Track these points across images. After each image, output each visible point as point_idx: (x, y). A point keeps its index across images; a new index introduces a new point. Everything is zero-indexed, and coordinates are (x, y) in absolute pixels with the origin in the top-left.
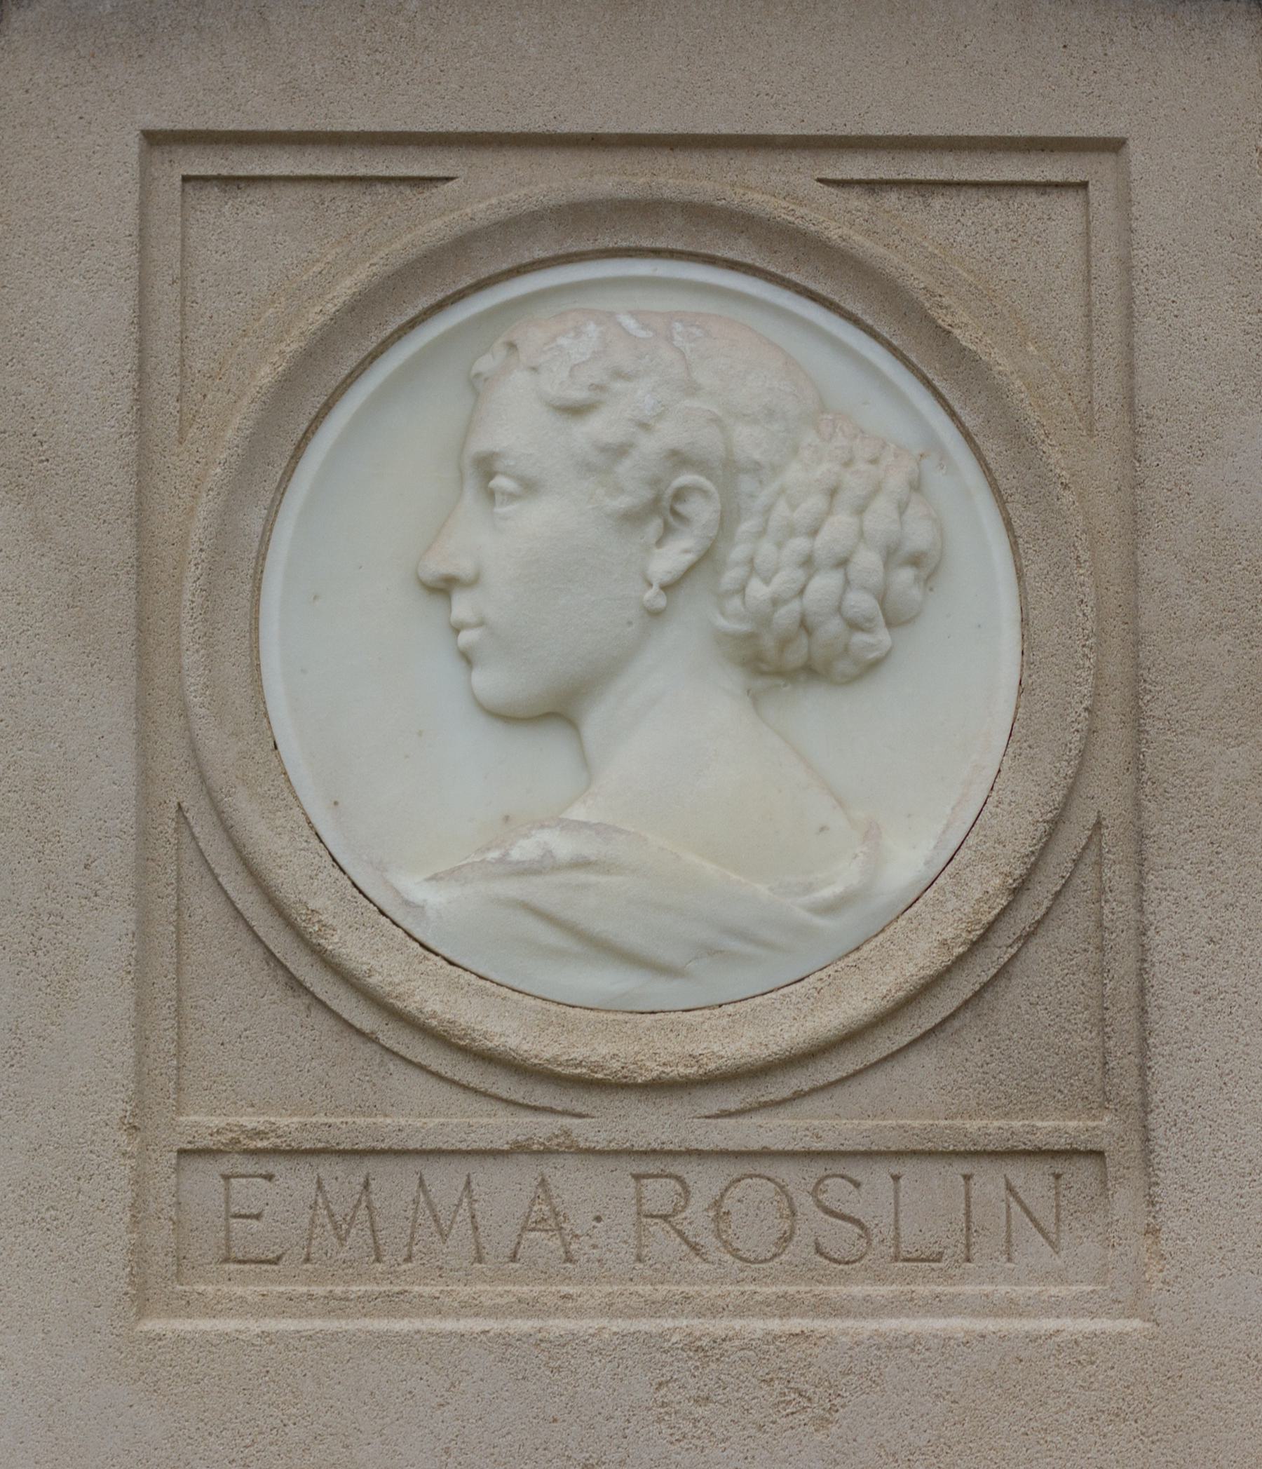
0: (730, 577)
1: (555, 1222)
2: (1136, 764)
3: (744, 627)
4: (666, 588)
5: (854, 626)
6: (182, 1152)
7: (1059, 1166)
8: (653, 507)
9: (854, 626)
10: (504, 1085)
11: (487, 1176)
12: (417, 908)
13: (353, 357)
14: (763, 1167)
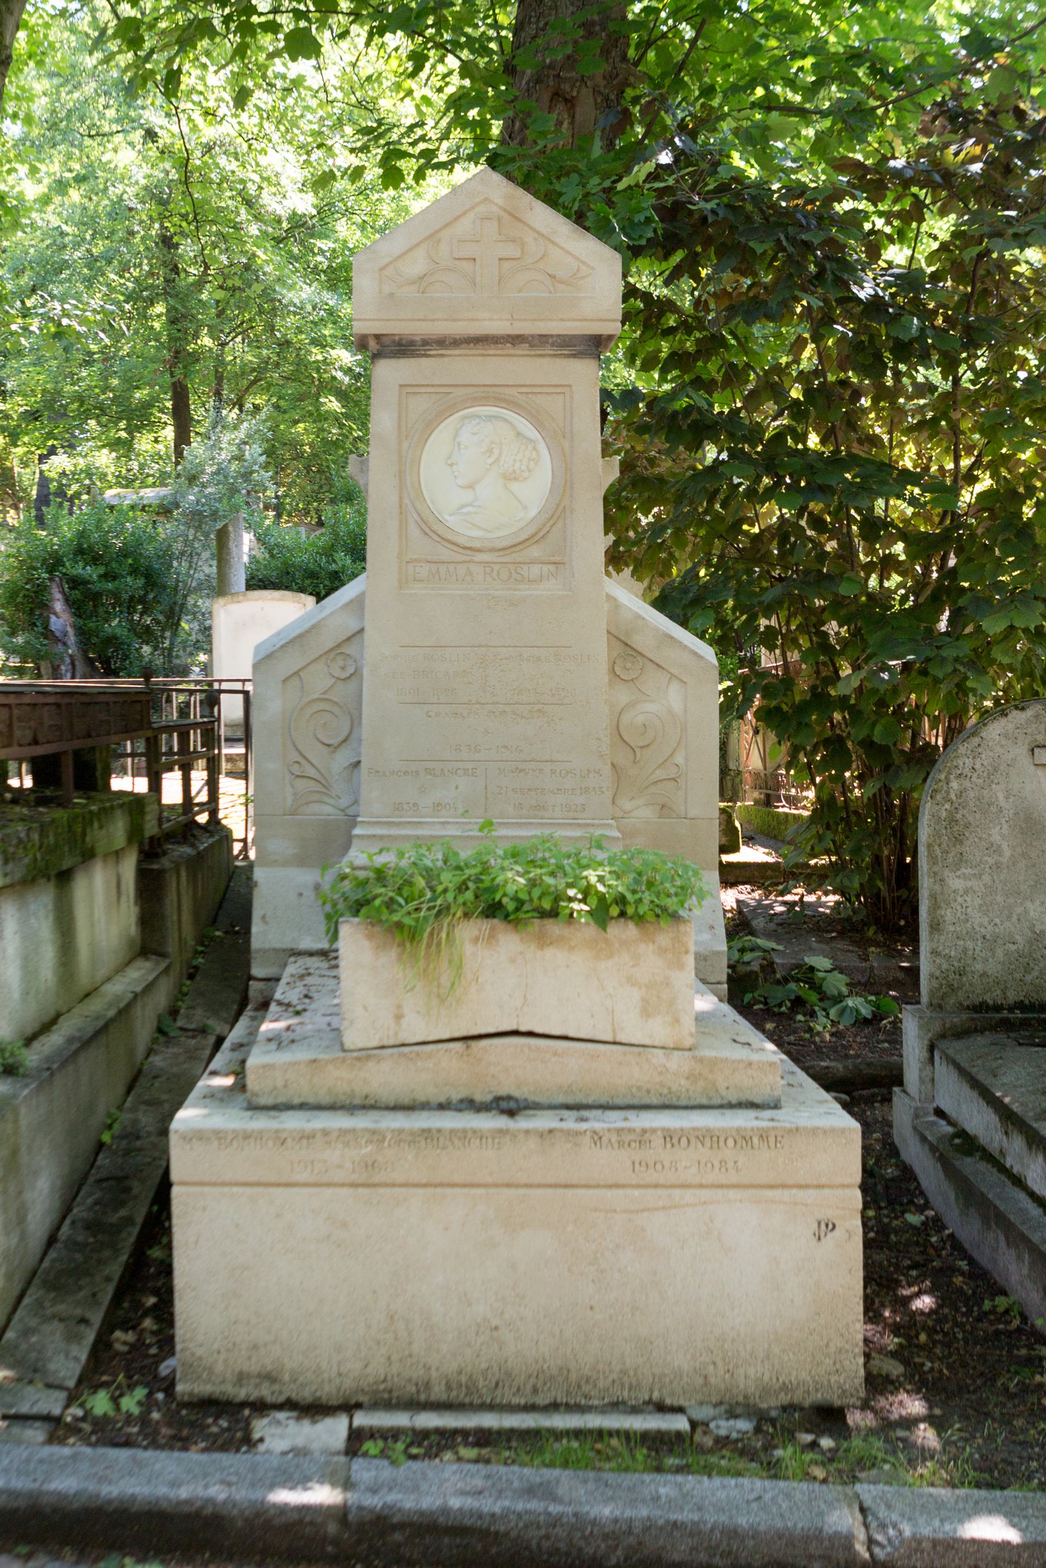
1: (470, 574)
2: (571, 496)
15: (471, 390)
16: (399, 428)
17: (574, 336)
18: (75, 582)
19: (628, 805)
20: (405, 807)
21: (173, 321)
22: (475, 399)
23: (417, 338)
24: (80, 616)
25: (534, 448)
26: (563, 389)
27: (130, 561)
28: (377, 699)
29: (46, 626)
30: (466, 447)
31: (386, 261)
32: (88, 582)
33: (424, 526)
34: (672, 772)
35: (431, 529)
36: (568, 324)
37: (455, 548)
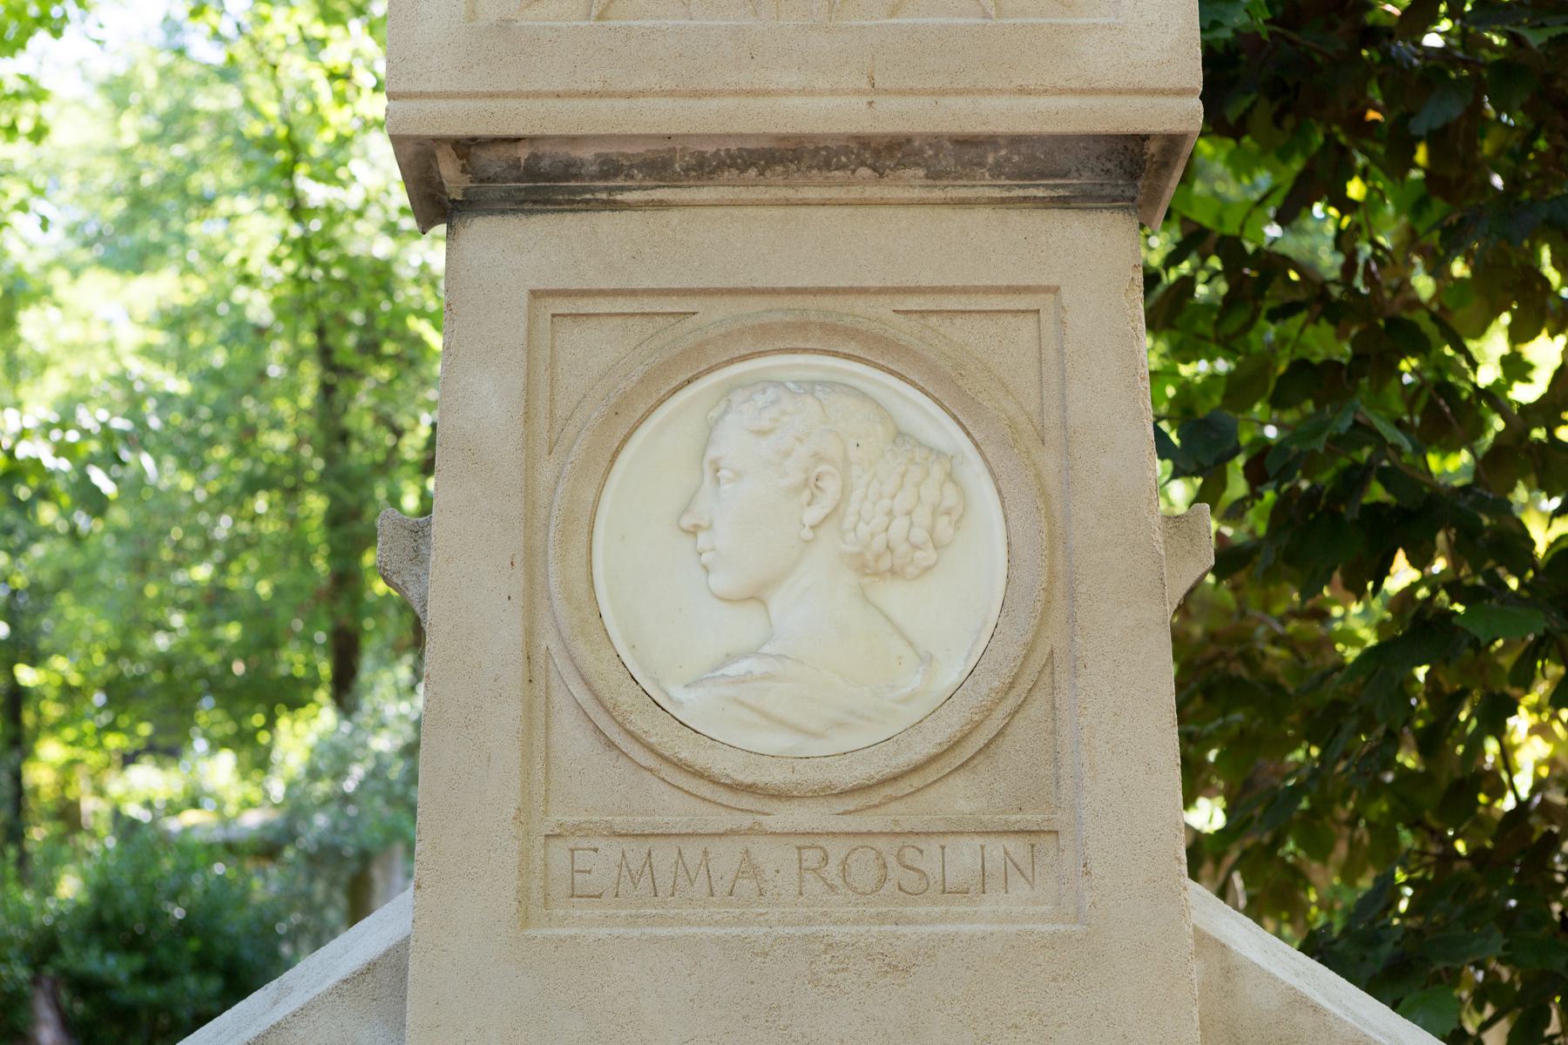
0: (849, 522)
1: (755, 872)
2: (1071, 619)
3: (856, 549)
4: (812, 527)
5: (916, 547)
6: (547, 836)
7: (1033, 839)
8: (806, 483)
9: (916, 547)
10: (725, 797)
11: (718, 847)
12: (679, 704)
13: (642, 408)
14: (869, 841)
16: (528, 417)
17: (1062, 140)
18: (85, 986)
22: (765, 330)
23: (587, 153)
25: (950, 477)
26: (1030, 299)
33: (603, 721)
35: (628, 728)
36: (1042, 102)
37: (704, 789)
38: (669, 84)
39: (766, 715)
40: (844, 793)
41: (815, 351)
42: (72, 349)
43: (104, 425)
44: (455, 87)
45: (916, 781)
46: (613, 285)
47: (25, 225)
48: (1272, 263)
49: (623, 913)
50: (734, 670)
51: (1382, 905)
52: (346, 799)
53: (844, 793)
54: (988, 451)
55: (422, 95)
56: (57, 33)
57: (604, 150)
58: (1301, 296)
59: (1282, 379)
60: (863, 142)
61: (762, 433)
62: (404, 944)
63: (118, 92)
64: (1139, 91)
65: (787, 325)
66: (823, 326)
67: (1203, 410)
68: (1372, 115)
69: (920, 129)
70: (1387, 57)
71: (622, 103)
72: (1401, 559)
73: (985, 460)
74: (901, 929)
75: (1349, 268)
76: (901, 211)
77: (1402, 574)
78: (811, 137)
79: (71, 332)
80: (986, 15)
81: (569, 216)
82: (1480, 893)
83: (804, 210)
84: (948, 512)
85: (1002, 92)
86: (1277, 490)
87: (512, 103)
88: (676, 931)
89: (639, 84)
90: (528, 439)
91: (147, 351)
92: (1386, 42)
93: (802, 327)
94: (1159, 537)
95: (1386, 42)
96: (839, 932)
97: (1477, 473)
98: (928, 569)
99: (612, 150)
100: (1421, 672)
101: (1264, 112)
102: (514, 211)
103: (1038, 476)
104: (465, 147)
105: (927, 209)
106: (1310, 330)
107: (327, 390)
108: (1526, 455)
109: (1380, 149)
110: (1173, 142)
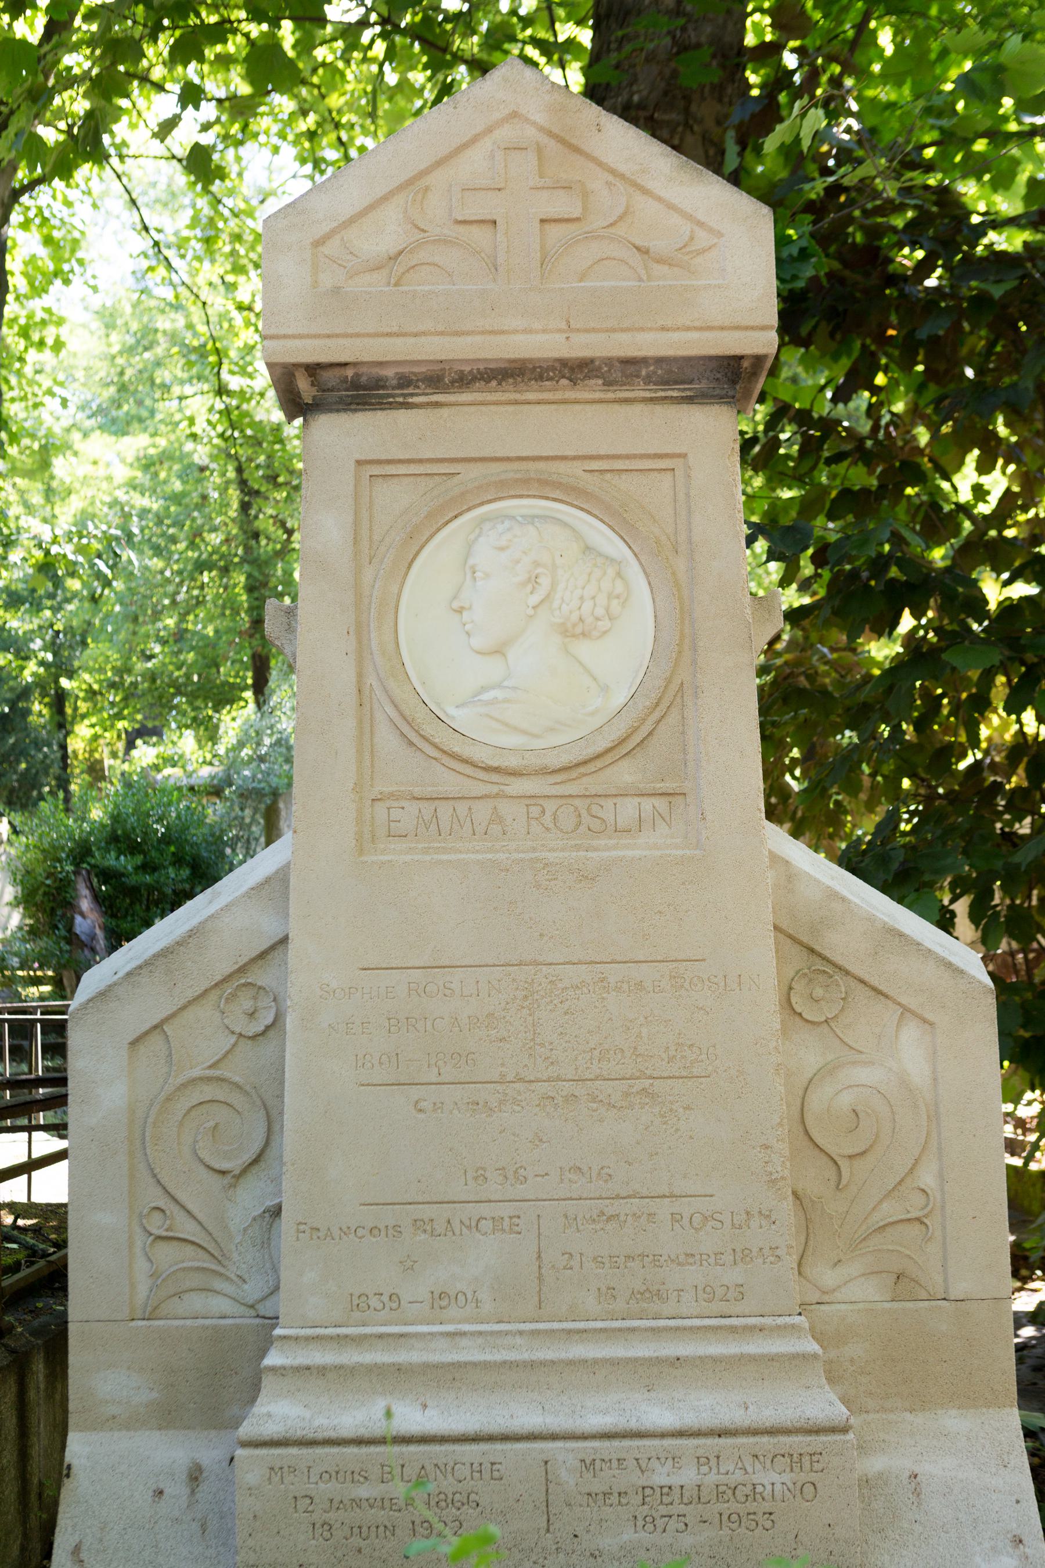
0: (556, 603)
1: (501, 820)
2: (694, 662)
5: (598, 619)
7: (670, 799)
8: (529, 580)
9: (598, 619)
10: (482, 775)
13: (427, 534)
14: (570, 801)
15: (495, 467)
16: (356, 541)
17: (688, 359)
18: (107, 875)
19: (829, 1277)
20: (374, 1302)
21: (250, 589)
22: (502, 484)
23: (389, 372)
24: (113, 916)
25: (619, 575)
26: (668, 461)
27: (172, 849)
28: (315, 1073)
29: (70, 929)
30: (487, 576)
31: (326, 227)
32: (123, 875)
33: (406, 729)
34: (915, 1206)
35: (421, 733)
36: (676, 336)
37: (468, 770)
38: (440, 328)
39: (507, 725)
40: (554, 772)
41: (534, 496)
42: (85, 481)
43: (104, 532)
44: (305, 331)
45: (599, 764)
46: (407, 457)
47: (52, 404)
48: (829, 425)
49: (420, 846)
50: (486, 696)
51: (891, 827)
52: (262, 759)
53: (554, 772)
54: (643, 558)
55: (285, 337)
56: (67, 282)
57: (400, 370)
58: (848, 447)
59: (833, 501)
60: (564, 363)
61: (502, 549)
62: (288, 865)
63: (109, 320)
64: (738, 328)
65: (516, 481)
66: (539, 481)
67: (786, 521)
68: (891, 332)
69: (598, 355)
70: (902, 295)
71: (412, 340)
72: (907, 612)
73: (641, 564)
74: (590, 854)
75: (876, 428)
76: (588, 407)
77: (907, 622)
78: (530, 360)
79: (84, 469)
80: (640, 280)
81: (379, 413)
82: (951, 820)
83: (527, 406)
84: (618, 597)
85: (651, 329)
86: (831, 570)
87: (341, 341)
88: (452, 857)
89: (421, 328)
90: (357, 553)
91: (133, 485)
92: (902, 285)
93: (526, 482)
94: (748, 611)
95: (902, 285)
96: (551, 856)
97: (953, 559)
98: (605, 632)
99: (405, 370)
100: (918, 684)
101: (824, 328)
102: (345, 410)
103: (674, 574)
104: (313, 369)
105: (604, 405)
106: (851, 471)
107: (245, 507)
108: (987, 549)
109: (896, 353)
110: (758, 360)
